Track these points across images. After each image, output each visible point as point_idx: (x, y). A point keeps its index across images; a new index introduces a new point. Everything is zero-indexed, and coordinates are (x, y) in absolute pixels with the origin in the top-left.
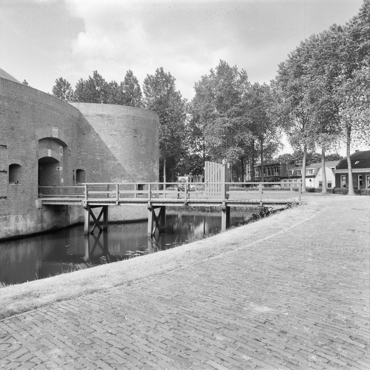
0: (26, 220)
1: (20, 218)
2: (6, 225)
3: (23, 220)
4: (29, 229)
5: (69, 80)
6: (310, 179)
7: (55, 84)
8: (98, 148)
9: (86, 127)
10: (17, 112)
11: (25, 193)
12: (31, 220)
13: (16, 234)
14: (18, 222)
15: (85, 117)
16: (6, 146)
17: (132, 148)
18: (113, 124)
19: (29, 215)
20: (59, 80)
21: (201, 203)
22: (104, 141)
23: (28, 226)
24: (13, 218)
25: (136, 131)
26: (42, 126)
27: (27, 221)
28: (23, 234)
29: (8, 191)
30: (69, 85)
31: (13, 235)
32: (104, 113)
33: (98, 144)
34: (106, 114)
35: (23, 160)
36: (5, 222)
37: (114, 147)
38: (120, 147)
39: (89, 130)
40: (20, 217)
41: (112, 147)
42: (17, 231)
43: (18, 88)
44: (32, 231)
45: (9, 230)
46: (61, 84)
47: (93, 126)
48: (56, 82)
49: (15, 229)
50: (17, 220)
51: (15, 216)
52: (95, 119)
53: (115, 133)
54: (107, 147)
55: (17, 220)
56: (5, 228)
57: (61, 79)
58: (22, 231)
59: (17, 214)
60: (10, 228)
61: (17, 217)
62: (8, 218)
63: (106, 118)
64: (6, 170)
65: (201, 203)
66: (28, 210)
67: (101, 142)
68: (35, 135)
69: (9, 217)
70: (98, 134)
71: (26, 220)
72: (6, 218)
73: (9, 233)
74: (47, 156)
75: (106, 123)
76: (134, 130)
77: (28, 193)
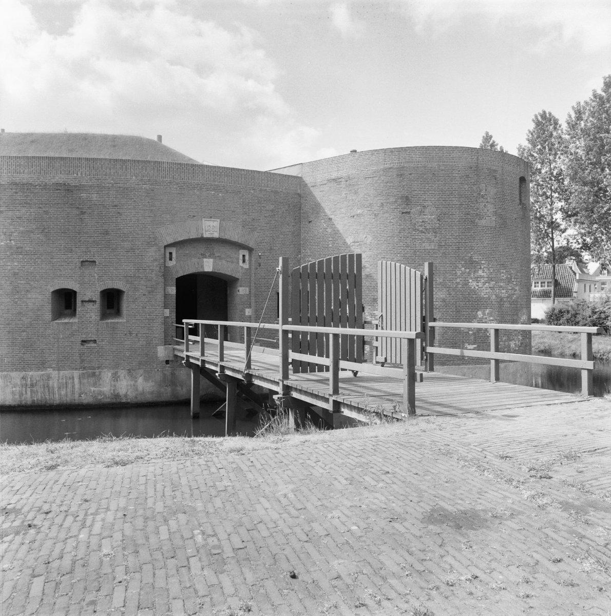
0: (134, 378)
1: (122, 375)
2: (95, 385)
3: (128, 378)
4: (143, 393)
5: (556, 114)
6: (331, 369)
7: (532, 126)
8: (331, 246)
9: (313, 208)
10: (116, 206)
11: (134, 335)
12: (146, 380)
13: (114, 401)
14: (117, 380)
15: (311, 189)
16: (94, 262)
17: (396, 239)
18: (356, 193)
19: (141, 371)
20: (540, 118)
21: (306, 393)
22: (341, 231)
23: (140, 389)
24: (107, 375)
25: (407, 200)
26: (172, 222)
27: (136, 381)
28: (129, 401)
29: (97, 331)
30: (556, 123)
31: (108, 400)
32: (340, 174)
33: (330, 239)
34: (344, 175)
35: (127, 281)
36: (92, 380)
37: (359, 240)
38: (370, 239)
39: (318, 213)
40: (122, 373)
41: (354, 242)
42: (117, 396)
43: (118, 166)
44: (149, 398)
45: (100, 393)
46: (545, 124)
47: (323, 205)
48: (533, 121)
49: (112, 392)
50: (115, 377)
51: (112, 371)
52: (326, 188)
53: (359, 211)
54: (345, 243)
55: (115, 377)
56: (93, 389)
57: (544, 115)
58: (126, 395)
59: (117, 366)
60: (101, 389)
61: (116, 373)
62: (97, 374)
63: (343, 184)
64: (94, 299)
65: (306, 393)
66: (140, 363)
67: (336, 232)
68: (155, 238)
69: (100, 372)
70: (330, 219)
71: (134, 378)
72: (94, 373)
73: (99, 397)
74: (201, 270)
75: (343, 195)
76: (402, 197)
77: (140, 335)
